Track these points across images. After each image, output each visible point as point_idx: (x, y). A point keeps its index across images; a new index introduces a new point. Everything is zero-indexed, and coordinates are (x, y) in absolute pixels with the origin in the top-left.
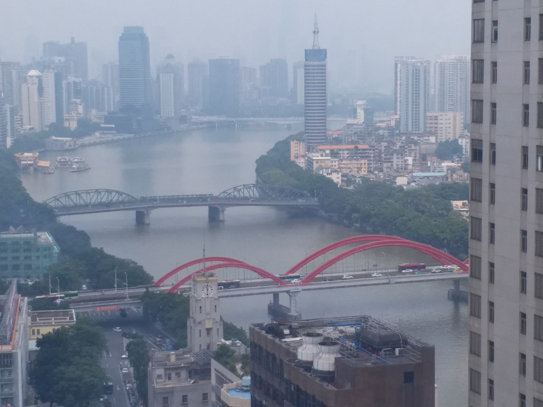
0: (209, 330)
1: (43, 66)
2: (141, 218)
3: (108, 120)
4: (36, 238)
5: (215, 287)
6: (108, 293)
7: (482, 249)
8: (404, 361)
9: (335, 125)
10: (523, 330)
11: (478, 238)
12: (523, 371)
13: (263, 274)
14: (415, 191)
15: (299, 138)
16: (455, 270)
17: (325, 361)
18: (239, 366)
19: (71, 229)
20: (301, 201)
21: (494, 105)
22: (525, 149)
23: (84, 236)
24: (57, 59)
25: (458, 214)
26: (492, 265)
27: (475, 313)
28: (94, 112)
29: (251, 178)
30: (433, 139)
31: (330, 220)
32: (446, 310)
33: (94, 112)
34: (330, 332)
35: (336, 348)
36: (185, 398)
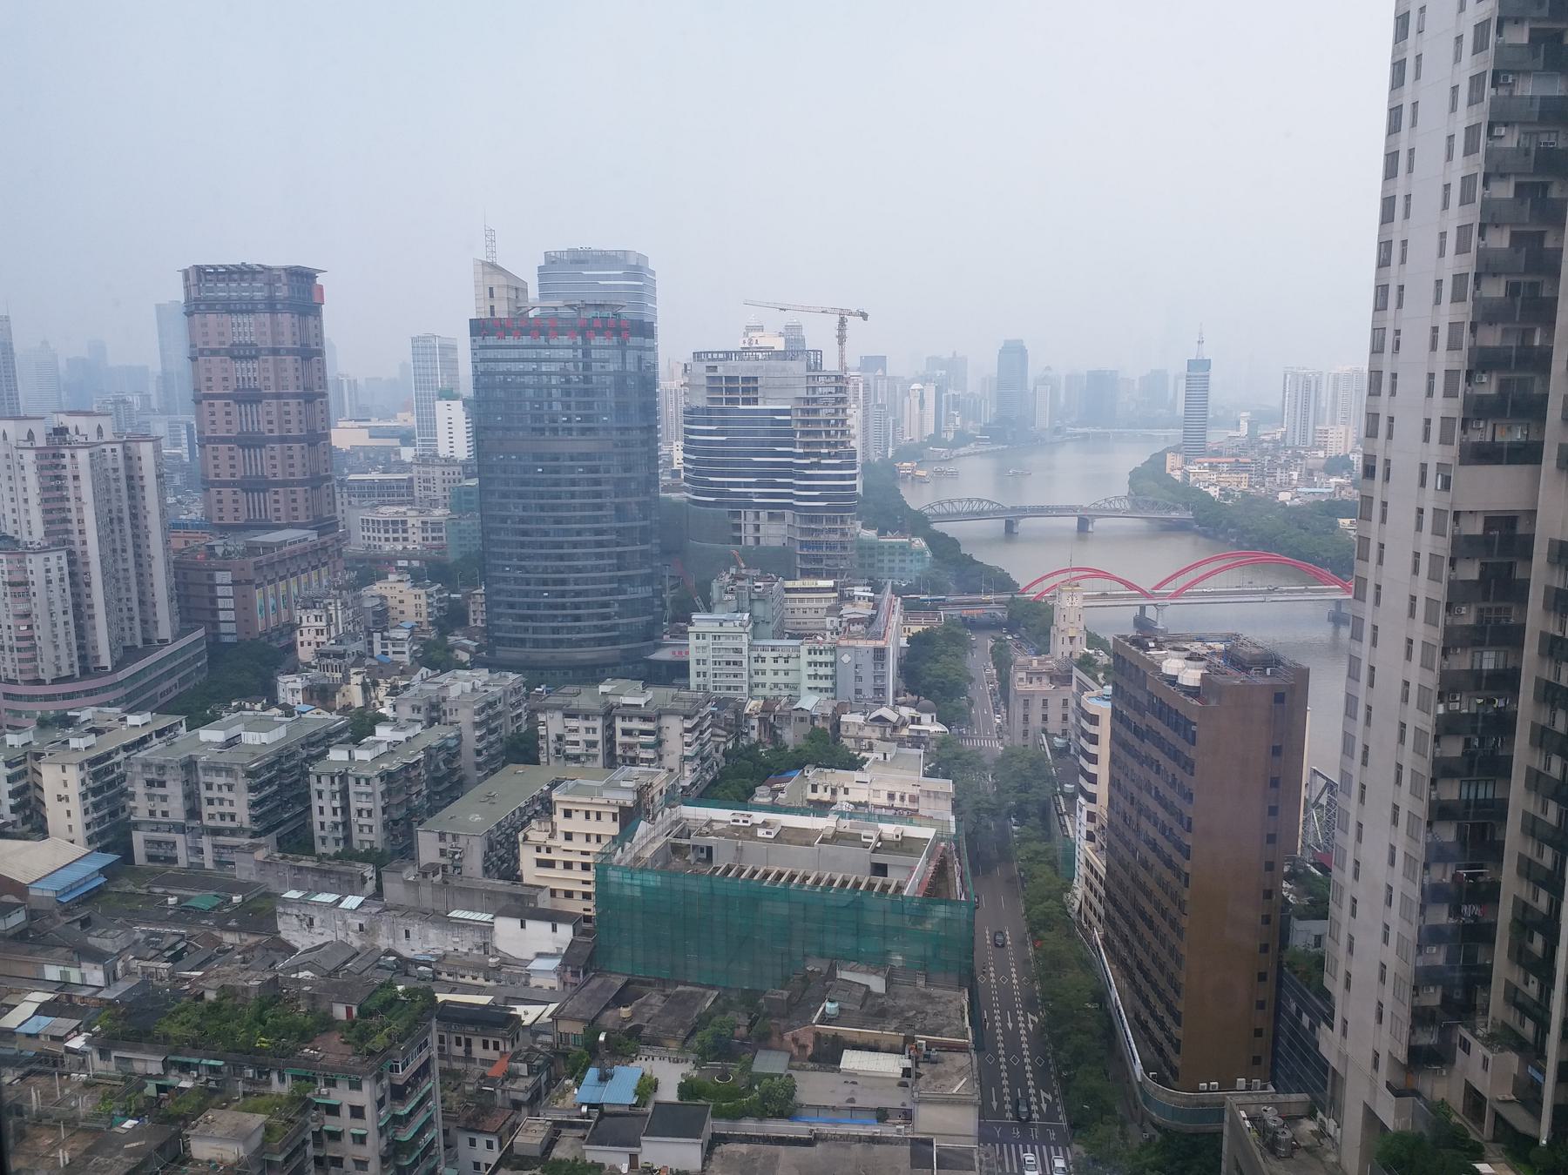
0: (1072, 639)
1: (925, 380)
2: (1010, 526)
3: (983, 431)
4: (911, 543)
5: (1080, 598)
6: (974, 597)
7: (1369, 570)
8: (1276, 681)
9: (1215, 437)
10: (1409, 656)
11: (1364, 558)
12: (1405, 699)
13: (1130, 586)
14: (1298, 507)
15: (1176, 450)
16: (1336, 593)
17: (1191, 676)
18: (1100, 675)
19: (943, 536)
20: (1174, 515)
21: (1391, 419)
22: (1424, 466)
23: (955, 543)
24: (938, 373)
25: (1345, 532)
26: (1378, 587)
27: (1356, 636)
28: (971, 423)
29: (1124, 490)
30: (1321, 454)
31: (1205, 535)
32: (1324, 632)
33: (971, 423)
34: (1197, 647)
35: (1203, 664)
36: (1045, 702)
